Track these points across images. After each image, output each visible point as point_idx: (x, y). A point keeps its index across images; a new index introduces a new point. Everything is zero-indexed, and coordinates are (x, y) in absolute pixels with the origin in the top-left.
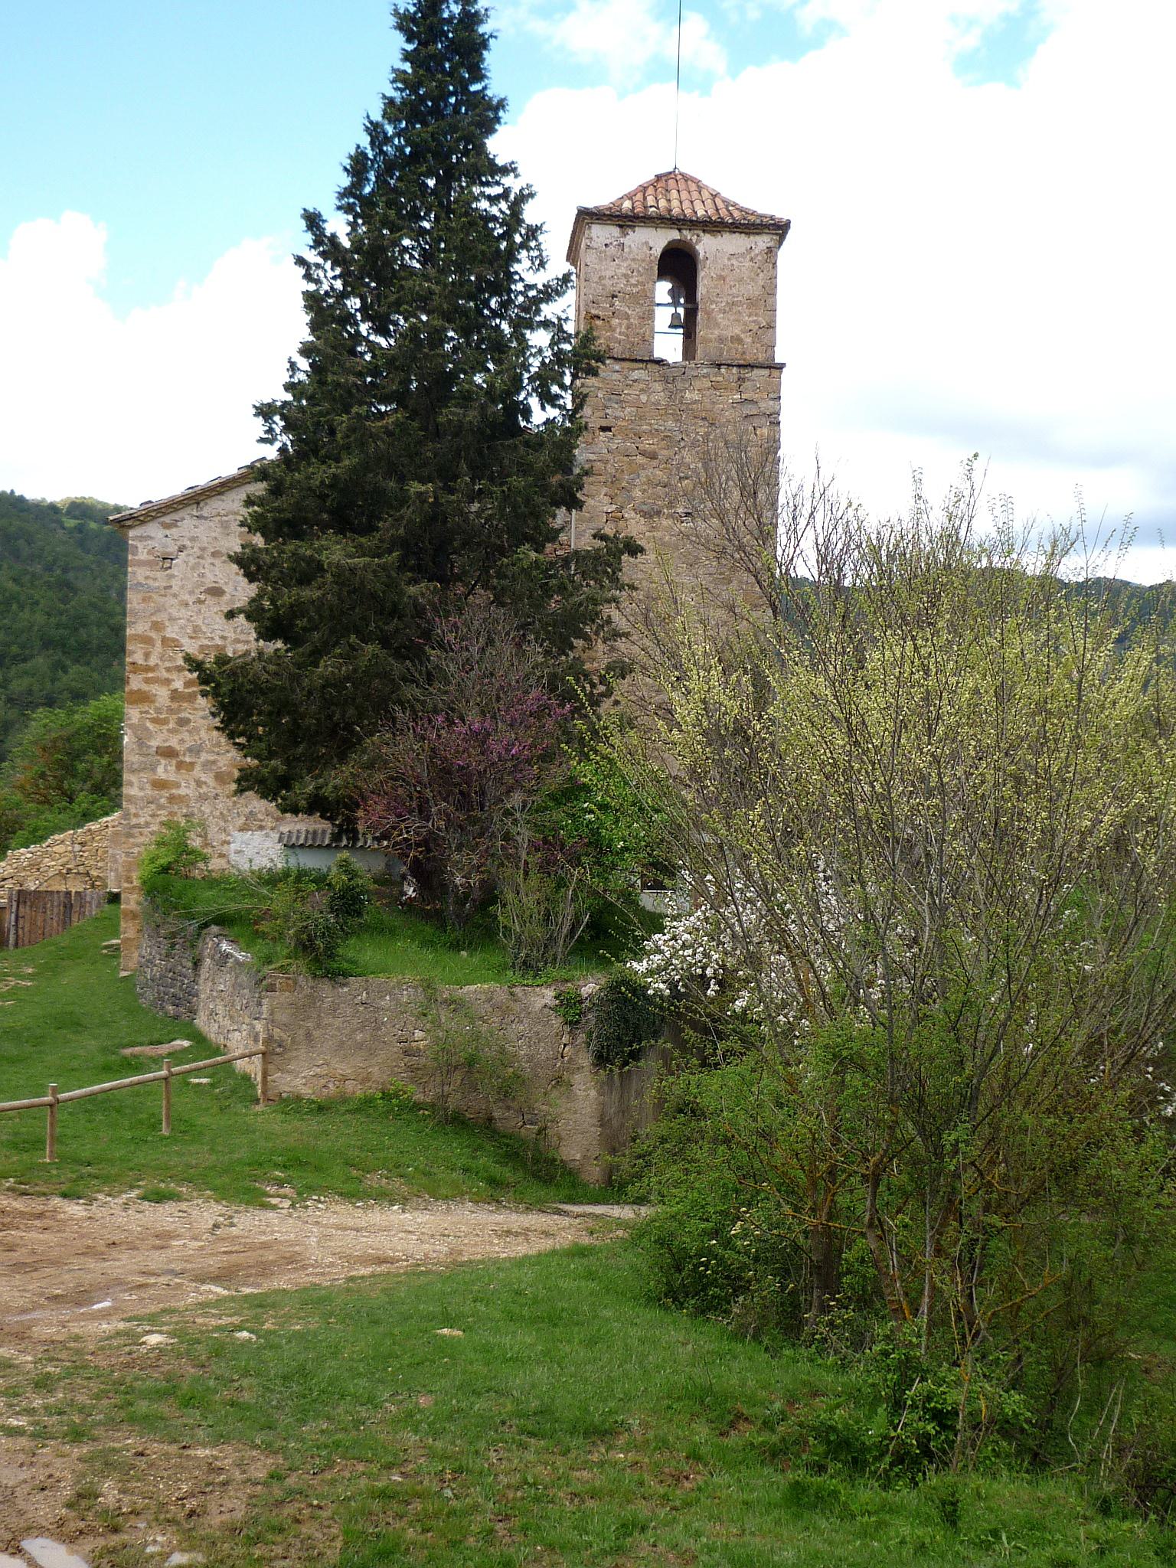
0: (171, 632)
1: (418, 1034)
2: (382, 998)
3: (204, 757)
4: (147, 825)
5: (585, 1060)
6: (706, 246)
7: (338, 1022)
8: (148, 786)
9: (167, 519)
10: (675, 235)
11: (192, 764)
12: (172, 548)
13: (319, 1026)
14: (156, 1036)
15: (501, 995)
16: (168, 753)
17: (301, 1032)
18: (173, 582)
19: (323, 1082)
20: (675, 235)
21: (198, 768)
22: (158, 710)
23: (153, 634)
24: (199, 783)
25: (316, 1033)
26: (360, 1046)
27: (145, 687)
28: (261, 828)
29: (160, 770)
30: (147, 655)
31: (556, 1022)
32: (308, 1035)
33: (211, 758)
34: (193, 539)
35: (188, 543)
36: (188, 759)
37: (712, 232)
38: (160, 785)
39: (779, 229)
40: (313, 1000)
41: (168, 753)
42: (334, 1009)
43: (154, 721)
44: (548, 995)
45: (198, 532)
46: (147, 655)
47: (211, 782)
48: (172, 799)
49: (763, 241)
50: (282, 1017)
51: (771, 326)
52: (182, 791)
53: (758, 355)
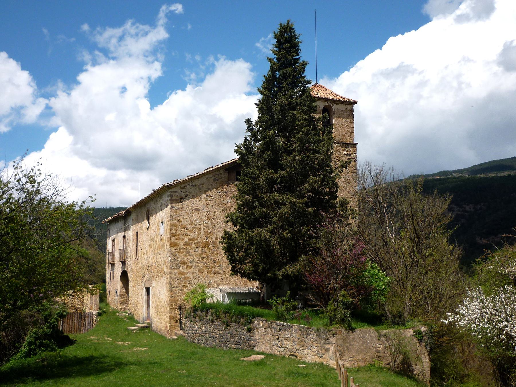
0: (184, 223)
1: (378, 346)
2: (366, 335)
3: (194, 264)
4: (177, 287)
5: (426, 354)
6: (335, 107)
7: (355, 344)
8: (177, 274)
9: (182, 186)
10: (326, 104)
11: (191, 267)
12: (184, 195)
13: (350, 345)
14: (246, 354)
15: (398, 332)
16: (184, 263)
17: (346, 347)
18: (184, 206)
19: (353, 362)
20: (326, 104)
21: (193, 268)
22: (180, 249)
23: (178, 224)
24: (193, 273)
25: (350, 347)
26: (363, 350)
27: (176, 241)
28: (213, 287)
29: (181, 269)
30: (176, 230)
31: (416, 340)
32: (348, 348)
33: (197, 264)
34: (190, 192)
35: (188, 194)
36: (189, 265)
37: (337, 104)
38: (181, 274)
39: (355, 103)
40: (347, 337)
41: (184, 263)
42: (354, 339)
43: (179, 252)
44: (411, 332)
45: (191, 190)
46: (176, 230)
47: (197, 272)
48: (185, 278)
49: (349, 107)
50: (340, 343)
51: (353, 132)
52: (188, 275)
53: (348, 140)
